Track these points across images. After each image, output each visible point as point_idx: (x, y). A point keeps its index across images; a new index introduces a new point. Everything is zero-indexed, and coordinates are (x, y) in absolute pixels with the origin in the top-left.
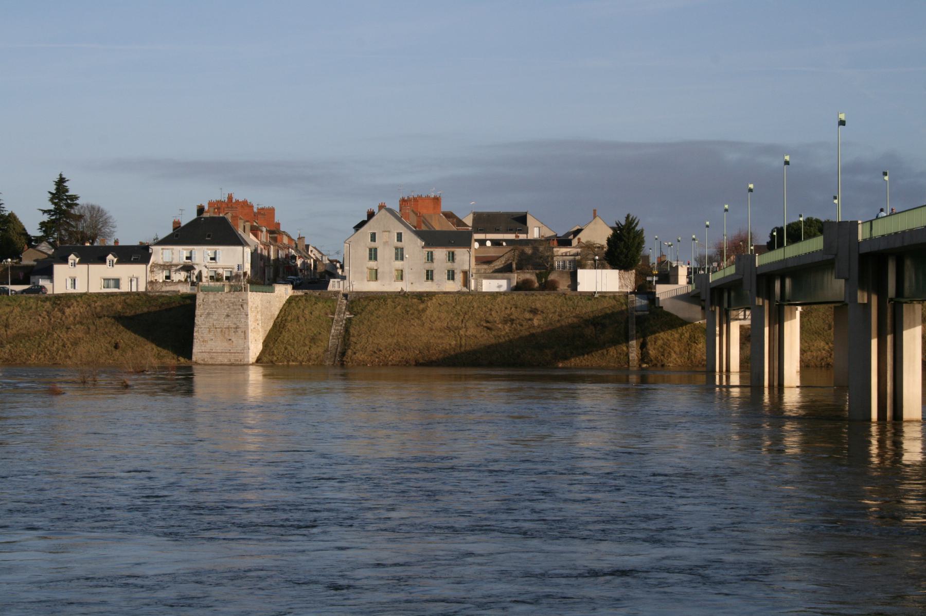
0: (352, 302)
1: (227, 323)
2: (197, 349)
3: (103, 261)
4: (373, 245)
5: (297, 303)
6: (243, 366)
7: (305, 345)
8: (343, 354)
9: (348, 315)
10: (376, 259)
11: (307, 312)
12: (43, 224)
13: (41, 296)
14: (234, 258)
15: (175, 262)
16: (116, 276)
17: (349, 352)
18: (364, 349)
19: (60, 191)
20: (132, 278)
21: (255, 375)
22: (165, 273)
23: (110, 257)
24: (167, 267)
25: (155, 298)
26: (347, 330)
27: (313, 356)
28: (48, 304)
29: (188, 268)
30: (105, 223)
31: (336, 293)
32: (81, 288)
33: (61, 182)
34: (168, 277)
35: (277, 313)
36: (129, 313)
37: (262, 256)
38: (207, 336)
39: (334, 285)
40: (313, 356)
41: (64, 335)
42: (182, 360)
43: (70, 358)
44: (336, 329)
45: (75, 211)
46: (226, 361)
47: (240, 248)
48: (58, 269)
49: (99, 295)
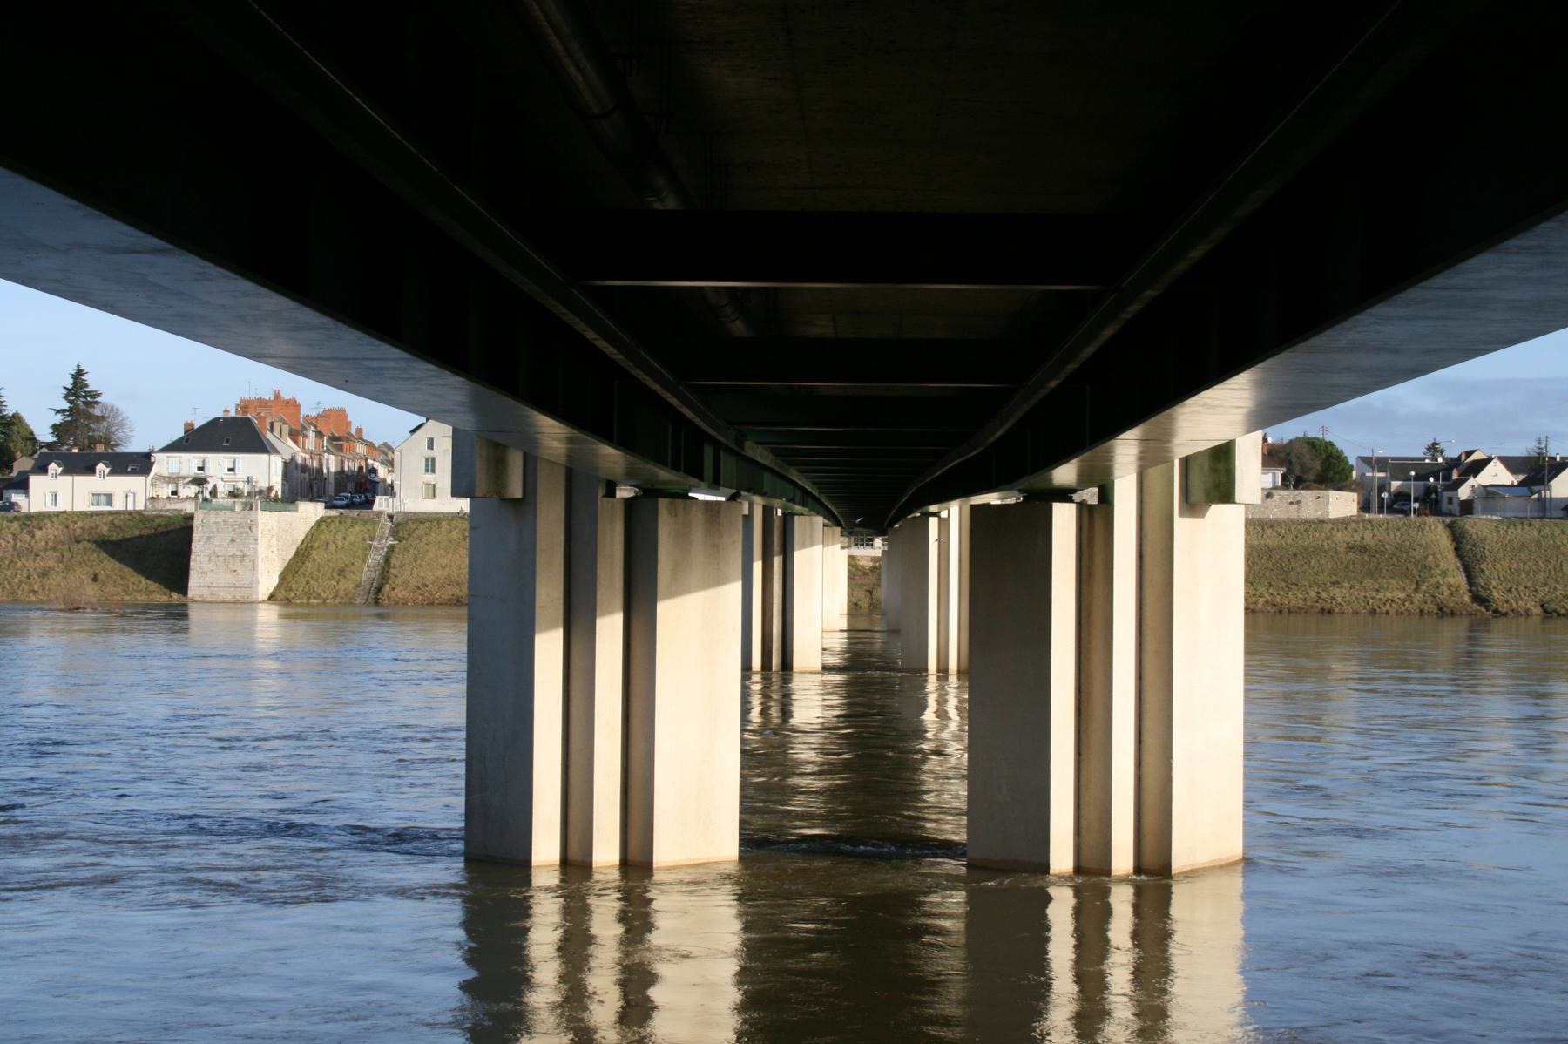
0: (398, 525)
1: (232, 550)
2: (194, 582)
3: (91, 470)
4: (430, 453)
5: (328, 526)
6: (253, 604)
7: (332, 578)
8: (379, 590)
9: (391, 541)
10: (433, 471)
11: (339, 537)
12: (55, 427)
13: (12, 514)
14: (265, 470)
15: (183, 473)
16: (107, 491)
17: (387, 587)
18: (406, 584)
19: (78, 387)
20: (129, 494)
21: (268, 615)
22: (171, 487)
23: (100, 467)
24: (174, 479)
25: (151, 519)
26: (387, 560)
27: (342, 593)
28: (16, 525)
29: (200, 482)
30: (121, 425)
31: (380, 514)
32: (64, 505)
33: (79, 374)
34: (174, 493)
35: (302, 538)
36: (115, 537)
37: (304, 468)
38: (207, 566)
39: (381, 503)
40: (342, 593)
41: (30, 565)
42: (175, 595)
43: (35, 592)
44: (374, 559)
45: (97, 411)
46: (229, 598)
47: (265, 456)
48: (34, 480)
49: (82, 514)
